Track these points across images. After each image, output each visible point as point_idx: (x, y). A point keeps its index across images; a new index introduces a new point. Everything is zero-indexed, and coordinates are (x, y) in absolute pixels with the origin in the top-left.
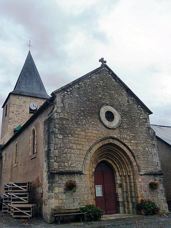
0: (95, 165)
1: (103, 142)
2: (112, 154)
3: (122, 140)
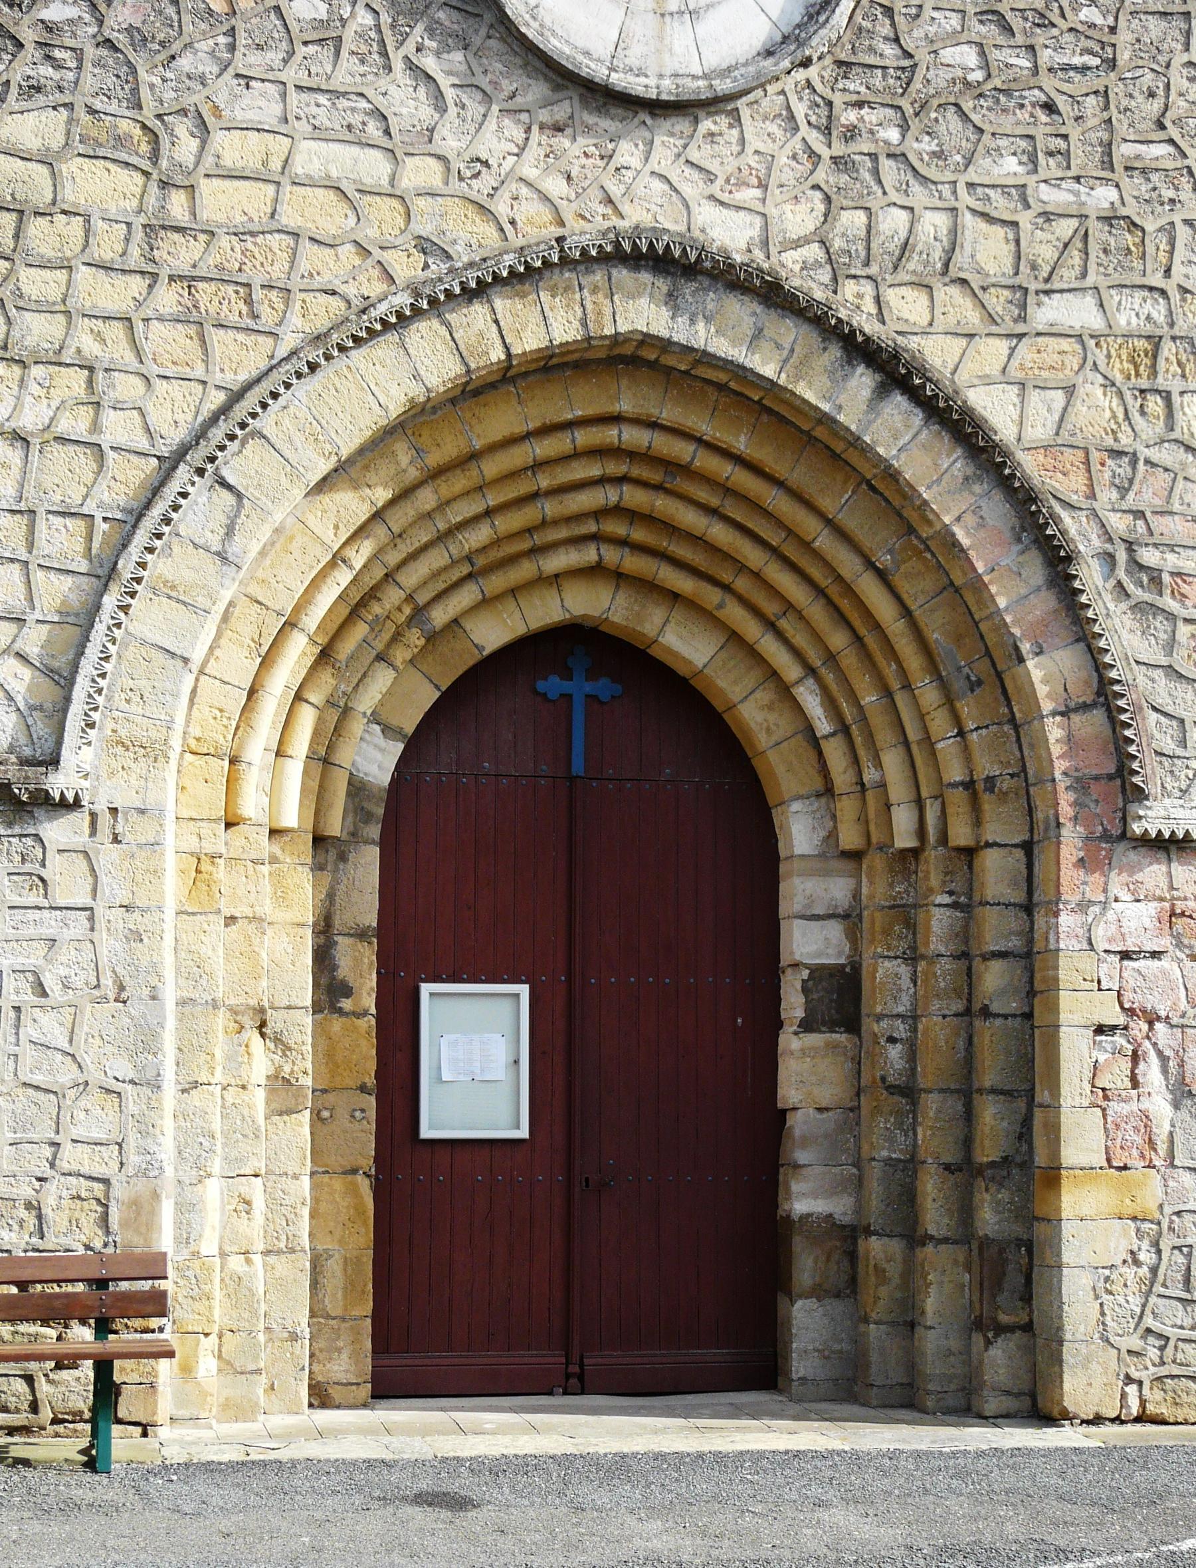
0: (398, 693)
1: (474, 320)
2: (689, 518)
3: (850, 289)
